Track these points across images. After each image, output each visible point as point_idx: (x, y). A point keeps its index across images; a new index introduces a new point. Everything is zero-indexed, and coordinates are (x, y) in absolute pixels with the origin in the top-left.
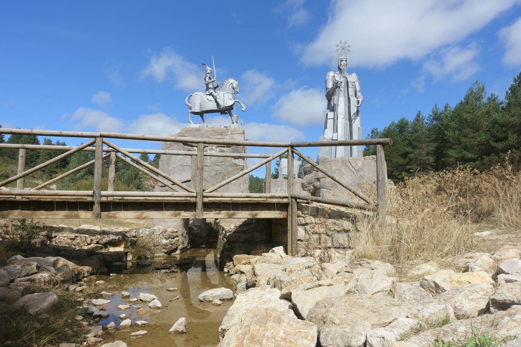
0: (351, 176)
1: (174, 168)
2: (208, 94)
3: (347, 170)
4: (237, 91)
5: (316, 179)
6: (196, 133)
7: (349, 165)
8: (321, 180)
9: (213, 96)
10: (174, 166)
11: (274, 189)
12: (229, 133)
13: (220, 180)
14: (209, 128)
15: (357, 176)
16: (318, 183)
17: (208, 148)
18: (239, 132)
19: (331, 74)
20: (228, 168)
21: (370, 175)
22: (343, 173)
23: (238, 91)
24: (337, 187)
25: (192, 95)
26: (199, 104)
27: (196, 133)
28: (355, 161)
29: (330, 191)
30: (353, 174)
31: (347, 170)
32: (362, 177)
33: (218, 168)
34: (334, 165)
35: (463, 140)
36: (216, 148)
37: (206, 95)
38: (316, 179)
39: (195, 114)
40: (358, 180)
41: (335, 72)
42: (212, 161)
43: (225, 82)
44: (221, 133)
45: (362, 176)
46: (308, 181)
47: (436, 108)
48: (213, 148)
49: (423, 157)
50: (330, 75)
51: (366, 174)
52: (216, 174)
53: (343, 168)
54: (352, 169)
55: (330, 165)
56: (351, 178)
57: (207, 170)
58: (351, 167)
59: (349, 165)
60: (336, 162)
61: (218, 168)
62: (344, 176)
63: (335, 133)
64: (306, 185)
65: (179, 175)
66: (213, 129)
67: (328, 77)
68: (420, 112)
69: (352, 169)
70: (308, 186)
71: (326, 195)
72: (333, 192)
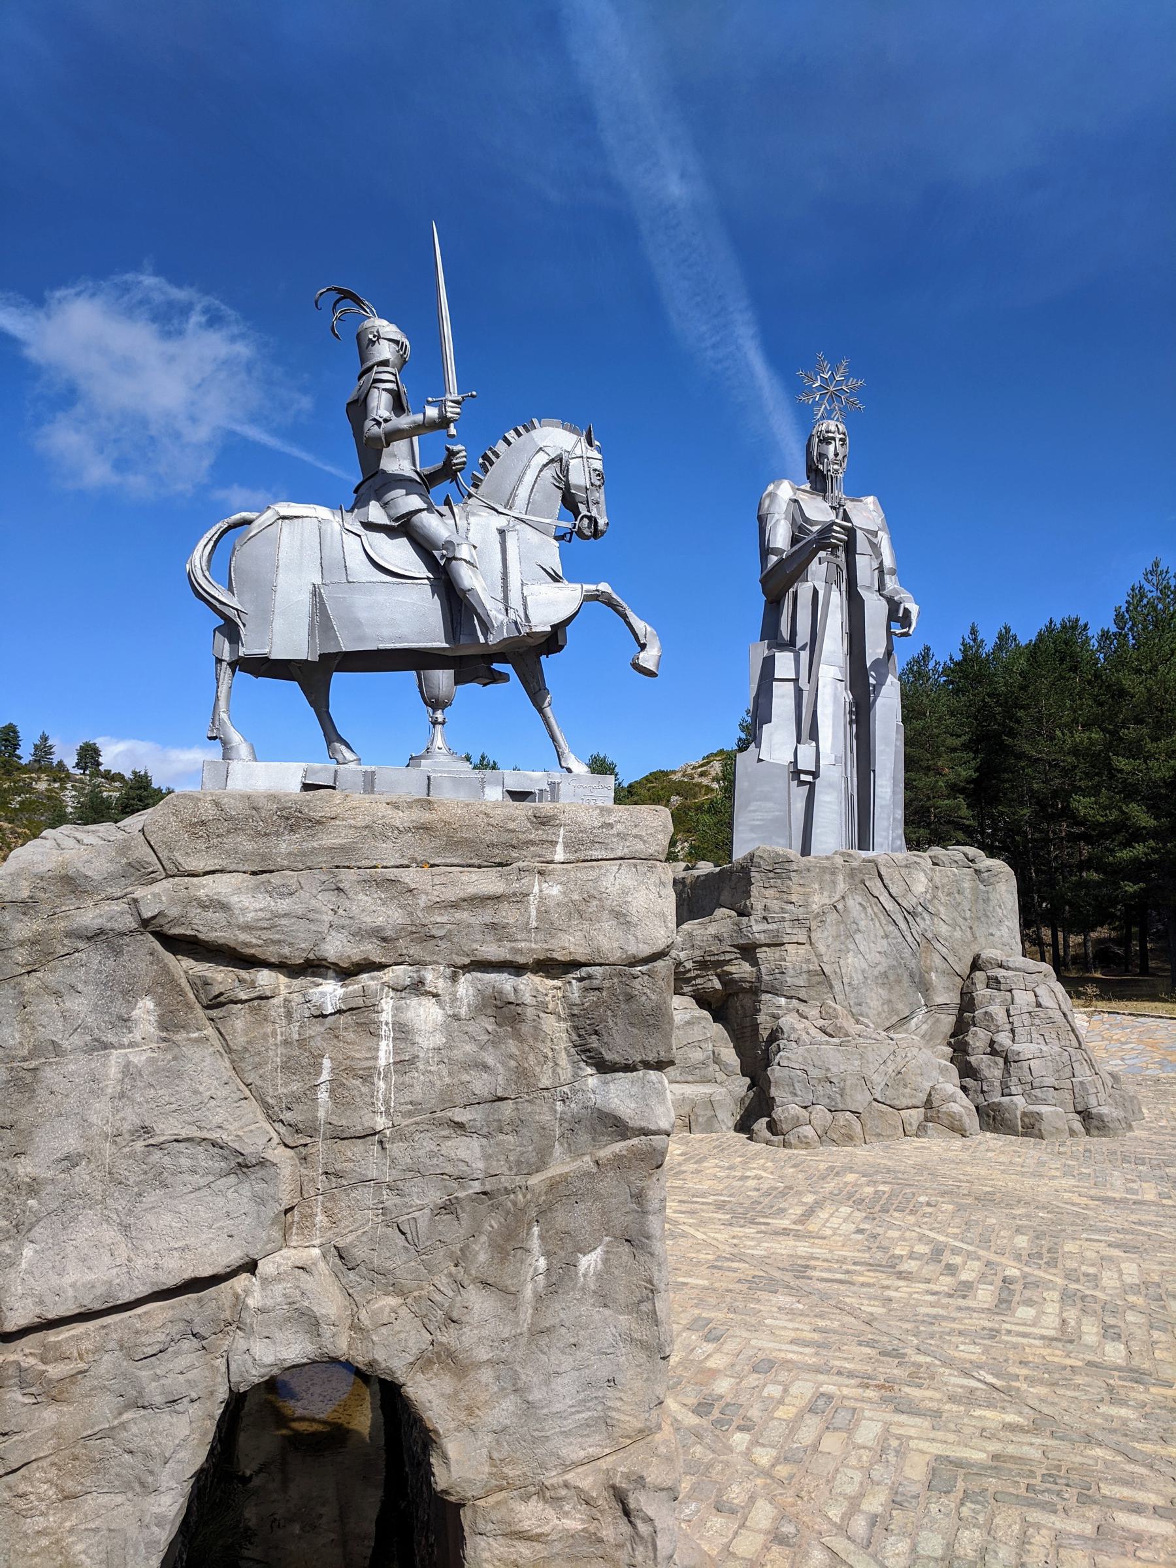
0: (887, 936)
1: (70, 1161)
2: (383, 520)
3: (869, 910)
4: (593, 521)
6: (283, 847)
7: (876, 887)
8: (762, 954)
9: (424, 546)
10: (72, 1143)
12: (560, 854)
13: (482, 1257)
14: (395, 806)
15: (910, 939)
16: (747, 967)
17: (388, 975)
19: (785, 491)
24: (831, 987)
25: (248, 522)
26: (305, 598)
27: (283, 847)
28: (903, 871)
30: (892, 928)
31: (869, 910)
32: (928, 941)
34: (817, 886)
35: (1121, 763)
36: (454, 978)
39: (257, 674)
40: (913, 954)
42: (418, 1093)
43: (501, 447)
45: (929, 935)
46: (698, 953)
47: (975, 640)
48: (429, 976)
51: (944, 929)
52: (449, 1207)
54: (890, 905)
56: (883, 944)
57: (373, 1173)
58: (884, 898)
59: (876, 887)
60: (827, 877)
61: (463, 1154)
62: (858, 937)
64: (689, 970)
65: (110, 1234)
66: (426, 817)
67: (772, 502)
68: (928, 649)
69: (890, 905)
70: (697, 976)
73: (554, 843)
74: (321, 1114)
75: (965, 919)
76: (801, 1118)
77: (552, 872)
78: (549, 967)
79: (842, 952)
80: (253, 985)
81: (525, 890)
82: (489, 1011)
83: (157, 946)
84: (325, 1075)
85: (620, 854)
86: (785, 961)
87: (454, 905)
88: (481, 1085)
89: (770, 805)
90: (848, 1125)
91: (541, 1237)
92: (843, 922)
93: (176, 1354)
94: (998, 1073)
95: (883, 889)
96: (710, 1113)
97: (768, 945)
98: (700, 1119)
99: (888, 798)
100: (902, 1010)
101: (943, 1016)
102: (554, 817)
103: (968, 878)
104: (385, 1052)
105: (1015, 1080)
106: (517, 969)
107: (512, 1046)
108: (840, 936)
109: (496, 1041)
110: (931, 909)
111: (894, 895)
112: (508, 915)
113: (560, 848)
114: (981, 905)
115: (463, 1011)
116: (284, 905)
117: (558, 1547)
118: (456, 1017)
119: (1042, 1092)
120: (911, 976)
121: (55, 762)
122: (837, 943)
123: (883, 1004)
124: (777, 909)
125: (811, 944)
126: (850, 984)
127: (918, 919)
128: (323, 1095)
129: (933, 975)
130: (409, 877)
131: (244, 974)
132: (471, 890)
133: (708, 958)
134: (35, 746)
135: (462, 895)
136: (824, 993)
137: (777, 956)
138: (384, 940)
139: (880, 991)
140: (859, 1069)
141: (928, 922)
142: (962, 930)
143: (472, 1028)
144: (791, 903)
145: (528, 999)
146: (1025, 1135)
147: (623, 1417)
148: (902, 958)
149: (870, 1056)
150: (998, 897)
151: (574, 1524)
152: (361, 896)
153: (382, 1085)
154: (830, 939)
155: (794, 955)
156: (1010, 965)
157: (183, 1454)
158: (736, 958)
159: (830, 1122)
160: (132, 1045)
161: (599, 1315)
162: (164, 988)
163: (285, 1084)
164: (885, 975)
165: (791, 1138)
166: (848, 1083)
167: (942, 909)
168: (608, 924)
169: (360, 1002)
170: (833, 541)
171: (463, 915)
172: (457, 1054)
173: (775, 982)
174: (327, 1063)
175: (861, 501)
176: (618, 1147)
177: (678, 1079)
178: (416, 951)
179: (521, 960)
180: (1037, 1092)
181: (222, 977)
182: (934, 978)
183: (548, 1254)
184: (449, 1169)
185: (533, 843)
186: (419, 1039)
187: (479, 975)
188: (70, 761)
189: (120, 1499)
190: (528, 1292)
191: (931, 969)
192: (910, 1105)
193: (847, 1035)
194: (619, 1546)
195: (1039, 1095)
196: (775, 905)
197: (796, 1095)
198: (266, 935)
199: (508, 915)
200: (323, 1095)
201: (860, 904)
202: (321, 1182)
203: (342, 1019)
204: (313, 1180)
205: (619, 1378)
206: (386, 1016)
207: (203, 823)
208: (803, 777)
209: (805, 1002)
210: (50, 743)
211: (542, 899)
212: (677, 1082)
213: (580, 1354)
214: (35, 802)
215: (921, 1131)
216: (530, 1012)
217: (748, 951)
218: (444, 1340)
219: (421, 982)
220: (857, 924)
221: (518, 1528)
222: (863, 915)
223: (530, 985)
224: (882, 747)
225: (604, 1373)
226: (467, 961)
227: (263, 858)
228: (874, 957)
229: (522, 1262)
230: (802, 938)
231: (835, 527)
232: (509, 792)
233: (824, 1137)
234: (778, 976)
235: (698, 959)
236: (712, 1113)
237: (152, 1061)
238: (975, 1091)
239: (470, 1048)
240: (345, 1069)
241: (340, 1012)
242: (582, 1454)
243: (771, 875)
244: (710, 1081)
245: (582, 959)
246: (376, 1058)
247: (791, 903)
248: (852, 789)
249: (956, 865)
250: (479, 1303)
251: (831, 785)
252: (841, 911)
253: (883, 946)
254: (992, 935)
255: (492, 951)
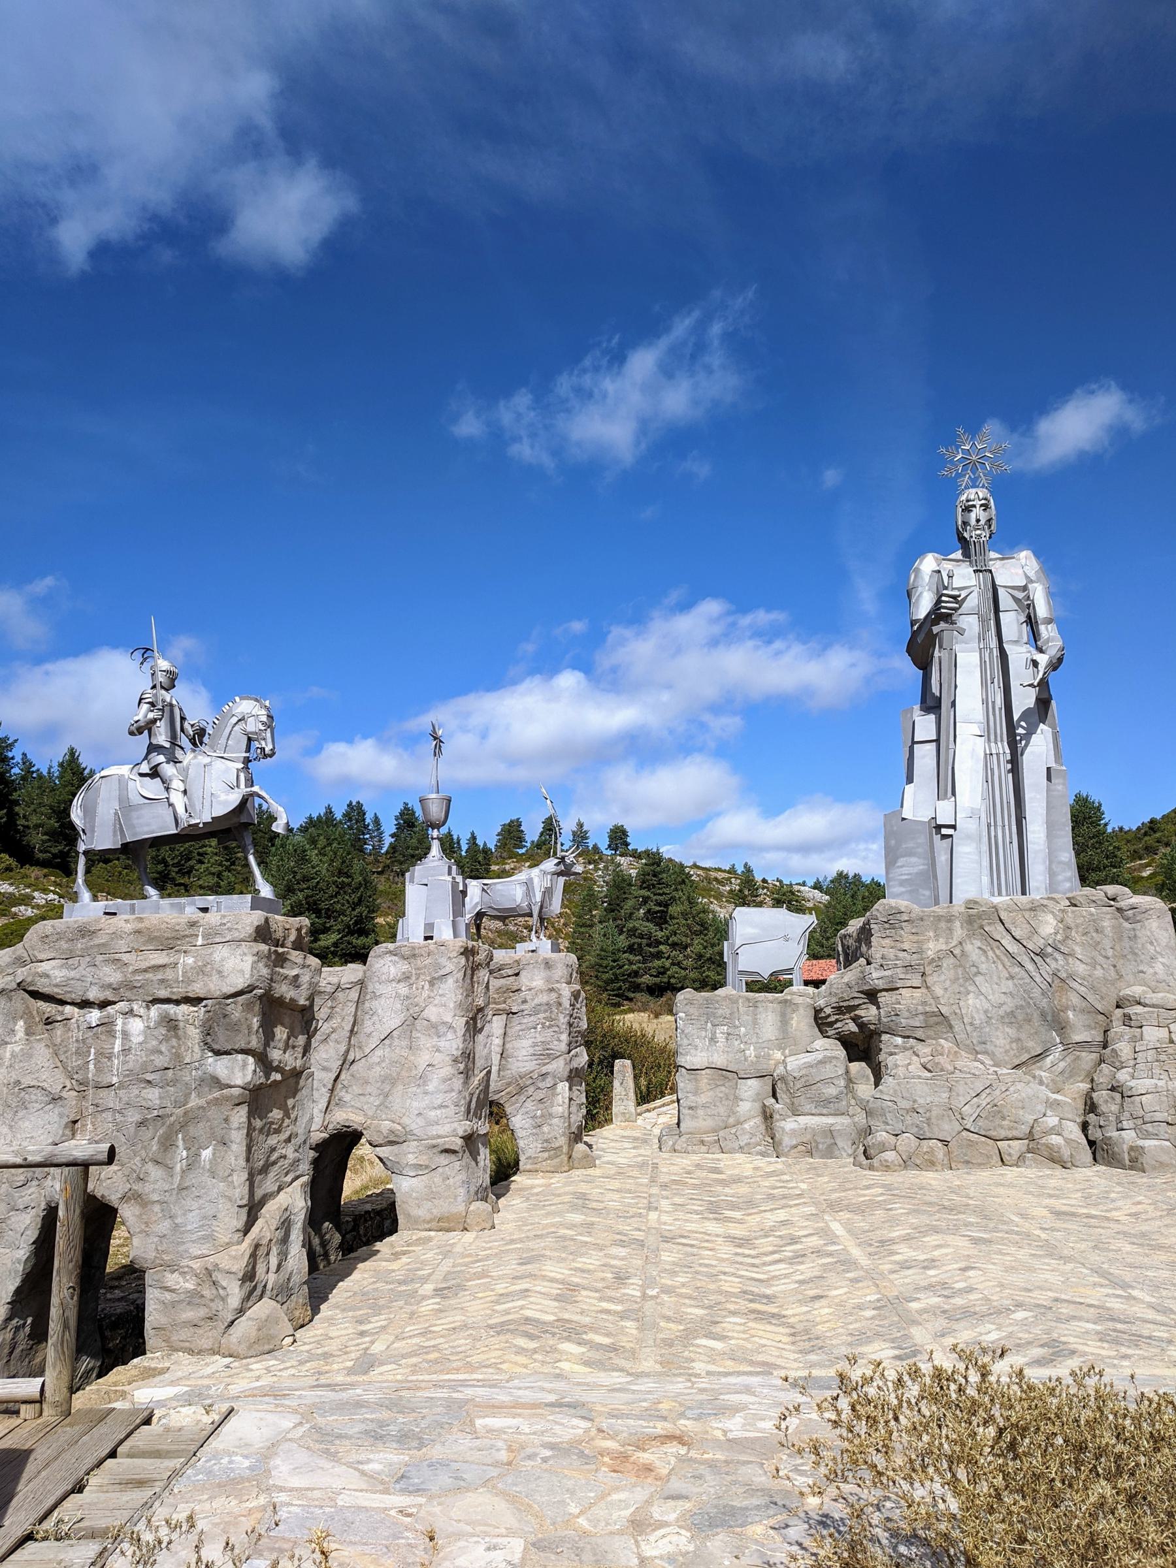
0: (1012, 977)
2: (147, 771)
3: (990, 953)
5: (861, 992)
7: (998, 931)
8: (883, 998)
11: (703, 1034)
12: (200, 941)
15: (1038, 979)
16: (873, 1010)
17: (117, 1007)
18: (236, 935)
20: (187, 1096)
21: (1099, 972)
22: (974, 969)
23: (267, 750)
24: (951, 1027)
26: (112, 817)
28: (1027, 914)
29: (919, 1047)
30: (1017, 969)
31: (990, 953)
32: (1060, 982)
33: (153, 1095)
34: (931, 934)
36: (148, 1008)
37: (137, 778)
38: (861, 992)
40: (1044, 993)
41: (944, 552)
42: (131, 1065)
44: (168, 939)
45: (1063, 975)
46: (834, 1000)
48: (135, 1007)
49: (861, 1189)
50: (922, 567)
51: (1081, 969)
52: (142, 1124)
53: (973, 948)
54: (1013, 948)
55: (915, 938)
58: (1007, 941)
59: (998, 931)
60: (943, 925)
61: (150, 1097)
62: (979, 979)
63: (945, 798)
64: (829, 1016)
66: (140, 926)
69: (1013, 948)
70: (837, 1021)
71: (896, 1066)
72: (928, 1050)
73: (197, 936)
74: (90, 1075)
75: (1108, 958)
76: (887, 1144)
77: (190, 951)
78: (195, 1001)
79: (962, 994)
80: (62, 1013)
81: (175, 961)
82: (164, 1024)
83: (27, 996)
84: (92, 1057)
85: (227, 939)
86: (900, 1003)
87: (145, 971)
88: (160, 1061)
89: (914, 860)
90: (931, 1151)
91: (183, 1139)
92: (961, 966)
93: (30, 1187)
94: (1114, 1108)
95: (1005, 933)
96: (829, 1141)
97: (887, 990)
98: (820, 1146)
99: (1042, 842)
100: (1033, 1048)
101: (1084, 1054)
102: (197, 922)
103: (1109, 916)
104: (118, 1046)
105: (1127, 1114)
106: (177, 1002)
107: (174, 1042)
108: (958, 979)
109: (166, 1039)
110: (1063, 949)
111: (1018, 938)
112: (169, 974)
113: (200, 938)
114: (1126, 943)
115: (152, 1024)
116: (72, 974)
117: (183, 1296)
118: (148, 1027)
119: (1153, 1127)
120: (1043, 1015)
121: (591, 846)
122: (956, 986)
123: (1011, 1042)
124: (892, 957)
125: (927, 988)
126: (971, 1024)
127: (1048, 960)
128: (91, 1066)
129: (1070, 1014)
130: (125, 958)
131: (60, 1008)
132: (153, 963)
133: (842, 1004)
134: (573, 832)
135: (149, 965)
136: (942, 1032)
137: (894, 1000)
138: (114, 989)
139: (1007, 1030)
140: (947, 1100)
141: (1061, 962)
142: (1103, 969)
143: (156, 1033)
144: (904, 950)
145: (180, 1018)
146: (1131, 1168)
147: (220, 1236)
148: (1031, 998)
149: (961, 1088)
150: (1149, 934)
151: (190, 1286)
152: (105, 968)
153: (116, 1061)
154: (948, 983)
155: (908, 999)
156: (1147, 1002)
157: (28, 1232)
158: (864, 1003)
159: (914, 1148)
160: (16, 1042)
161: (210, 1182)
162: (27, 1015)
163: (76, 1061)
164: (1012, 1014)
165: (875, 1162)
166: (934, 1113)
167: (1078, 950)
168: (215, 977)
169: (106, 1020)
170: (943, 611)
171: (149, 976)
172: (149, 1046)
173: (892, 1023)
174: (93, 1050)
175: (1014, 558)
176: (217, 1094)
177: (813, 1112)
178: (128, 994)
179: (175, 997)
180: (1148, 1127)
181: (49, 1008)
182: (1071, 1016)
183: (188, 1149)
184: (144, 1104)
185: (187, 936)
186: (132, 1039)
187: (160, 1005)
188: (603, 844)
189: (8, 1251)
190: (178, 1168)
191: (1067, 1008)
192: (1010, 1136)
193: (942, 1070)
194: (212, 1300)
195: (1151, 1129)
196: (891, 953)
197: (887, 1124)
198: (65, 989)
199: (169, 974)
200: (91, 1066)
201: (980, 948)
202: (91, 1109)
203: (100, 1029)
204: (87, 1108)
205: (219, 1216)
206: (119, 1028)
207: (47, 936)
208: (944, 831)
209: (924, 1041)
210: (585, 828)
211: (184, 965)
212: (813, 1115)
213: (201, 1201)
214: (574, 883)
215: (1020, 1161)
216: (181, 1024)
217: (872, 996)
218: (136, 1188)
219: (132, 1010)
220: (977, 967)
221: (166, 1285)
222: (983, 959)
223: (182, 1011)
224: (1033, 795)
225: (211, 1213)
226: (151, 999)
227: (71, 951)
228: (997, 998)
229: (175, 1152)
230: (917, 982)
231: (944, 598)
232: (199, 909)
233: (906, 1163)
234: (894, 1018)
235: (834, 1005)
236: (832, 1141)
237: (22, 1049)
238: (1094, 1126)
239: (154, 1043)
240: (100, 1054)
241: (98, 1025)
242: (200, 1252)
243: (887, 926)
244: (843, 1114)
245: (202, 996)
246: (113, 1048)
247: (904, 950)
248: (1011, 837)
249: (1095, 905)
250: (155, 1172)
251: (968, 837)
252: (958, 956)
253: (1008, 987)
254: (1142, 972)
255: (163, 993)
